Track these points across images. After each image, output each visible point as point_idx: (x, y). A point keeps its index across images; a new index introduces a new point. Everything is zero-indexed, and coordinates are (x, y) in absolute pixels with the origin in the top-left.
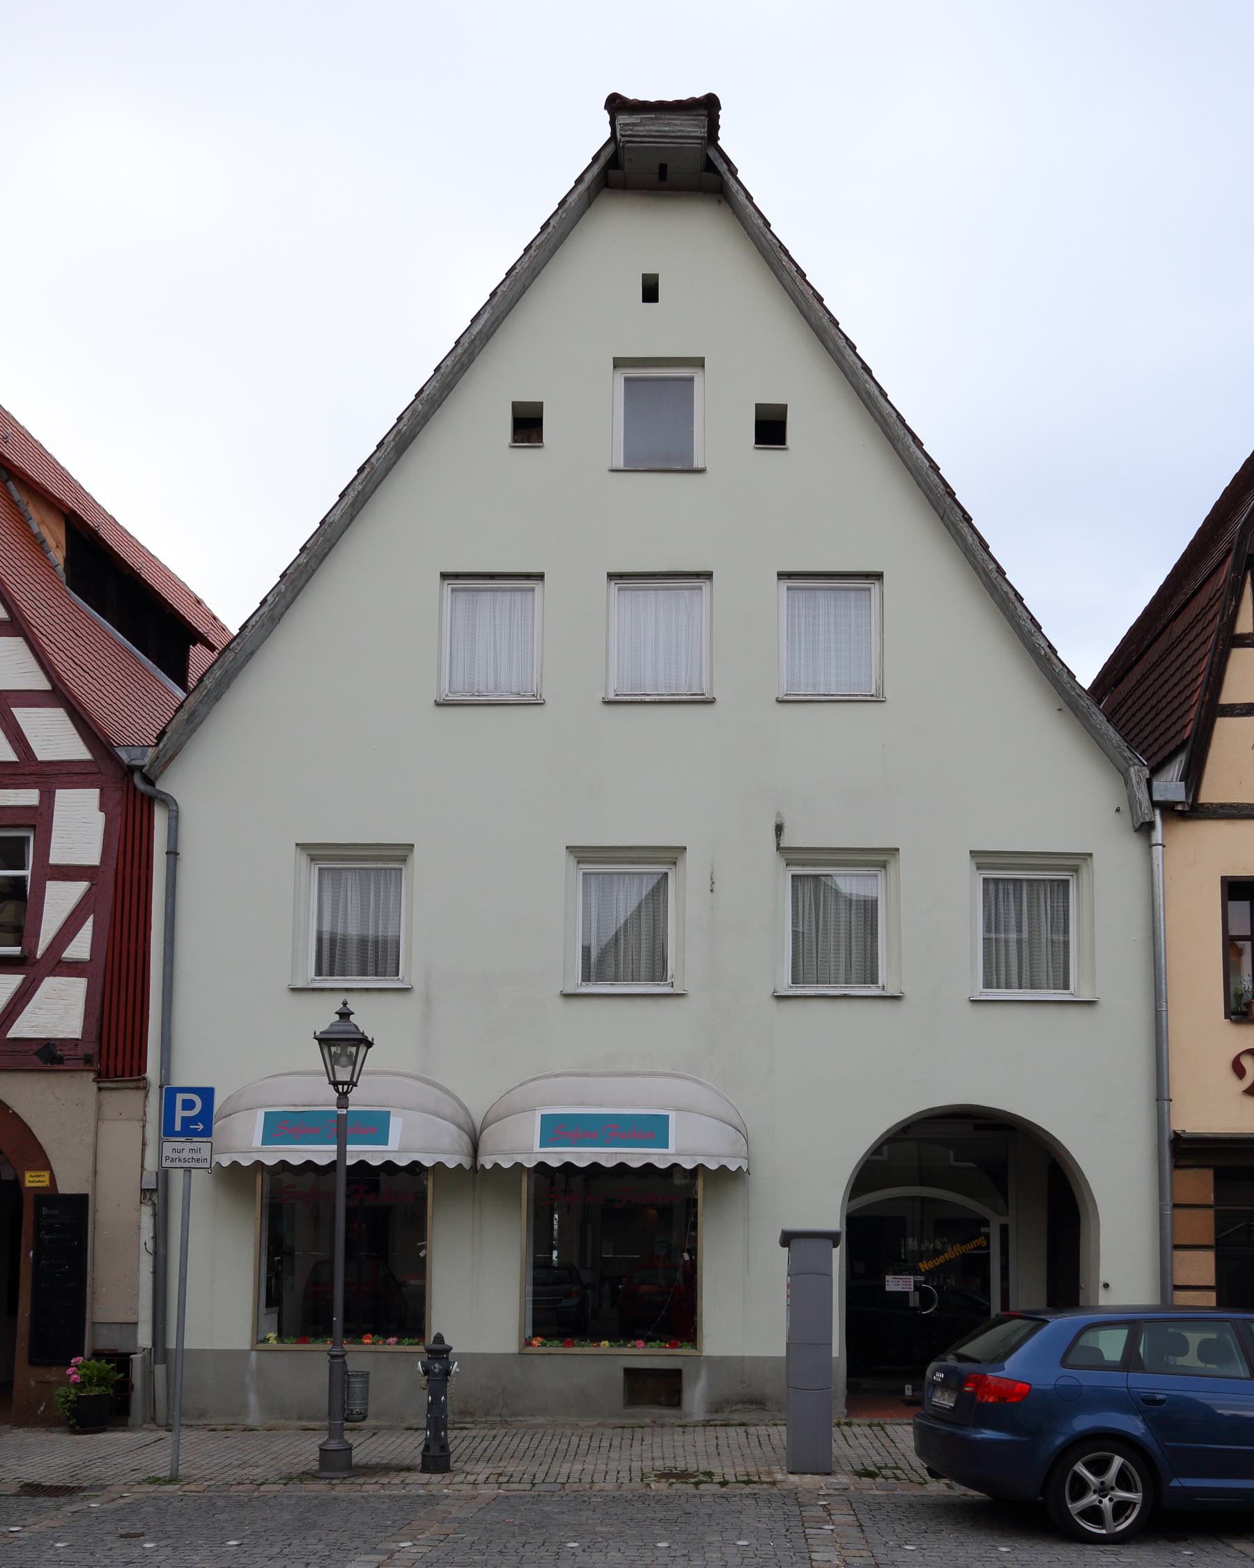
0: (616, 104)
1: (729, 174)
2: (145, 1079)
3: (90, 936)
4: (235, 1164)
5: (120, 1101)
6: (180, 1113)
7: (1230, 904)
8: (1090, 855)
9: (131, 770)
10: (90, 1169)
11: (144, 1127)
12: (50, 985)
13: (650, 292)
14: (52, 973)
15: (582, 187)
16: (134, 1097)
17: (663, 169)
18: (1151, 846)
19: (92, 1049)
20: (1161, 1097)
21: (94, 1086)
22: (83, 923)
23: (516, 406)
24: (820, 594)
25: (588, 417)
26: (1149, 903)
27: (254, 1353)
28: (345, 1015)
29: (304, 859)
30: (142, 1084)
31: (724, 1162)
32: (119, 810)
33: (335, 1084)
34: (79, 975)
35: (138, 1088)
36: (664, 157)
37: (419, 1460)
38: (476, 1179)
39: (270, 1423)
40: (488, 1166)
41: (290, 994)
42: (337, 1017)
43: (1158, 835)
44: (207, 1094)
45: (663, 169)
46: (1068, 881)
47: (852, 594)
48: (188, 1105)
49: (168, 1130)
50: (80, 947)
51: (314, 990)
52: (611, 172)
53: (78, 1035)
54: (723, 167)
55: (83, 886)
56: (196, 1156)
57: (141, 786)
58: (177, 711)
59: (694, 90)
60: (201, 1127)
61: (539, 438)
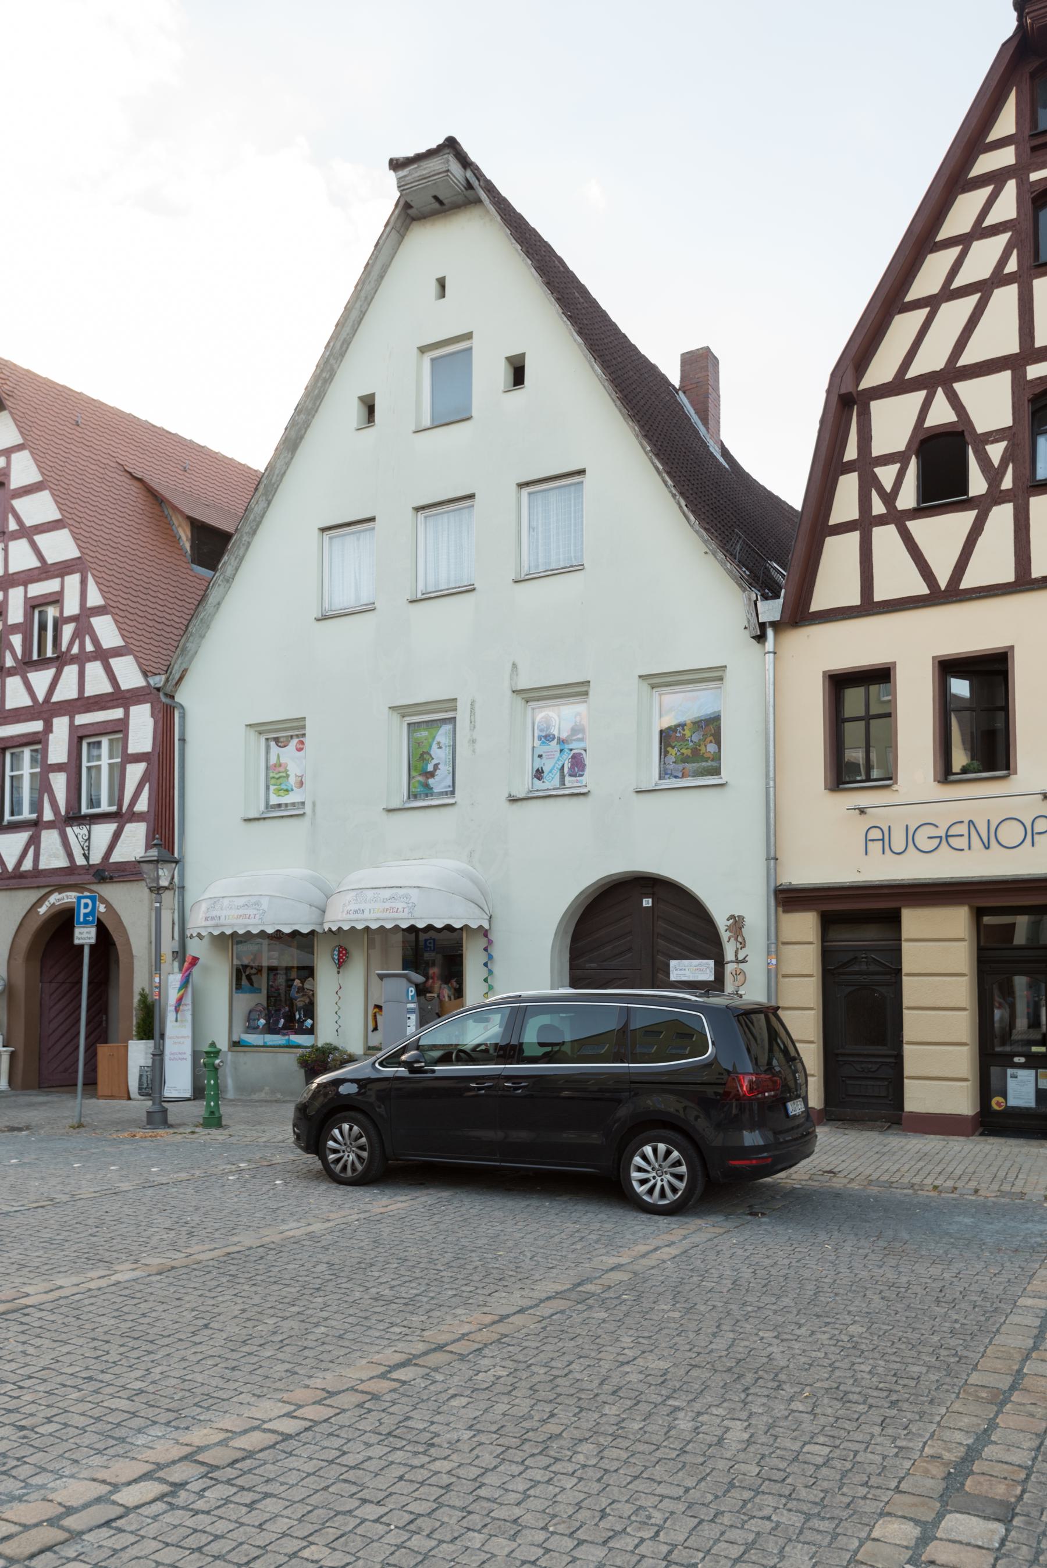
0: (396, 165)
4: (223, 933)
12: (129, 827)
14: (130, 821)
15: (388, 229)
20: (773, 859)
24: (551, 493)
29: (645, 686)
32: (161, 715)
36: (441, 187)
43: (770, 644)
50: (142, 805)
51: (264, 819)
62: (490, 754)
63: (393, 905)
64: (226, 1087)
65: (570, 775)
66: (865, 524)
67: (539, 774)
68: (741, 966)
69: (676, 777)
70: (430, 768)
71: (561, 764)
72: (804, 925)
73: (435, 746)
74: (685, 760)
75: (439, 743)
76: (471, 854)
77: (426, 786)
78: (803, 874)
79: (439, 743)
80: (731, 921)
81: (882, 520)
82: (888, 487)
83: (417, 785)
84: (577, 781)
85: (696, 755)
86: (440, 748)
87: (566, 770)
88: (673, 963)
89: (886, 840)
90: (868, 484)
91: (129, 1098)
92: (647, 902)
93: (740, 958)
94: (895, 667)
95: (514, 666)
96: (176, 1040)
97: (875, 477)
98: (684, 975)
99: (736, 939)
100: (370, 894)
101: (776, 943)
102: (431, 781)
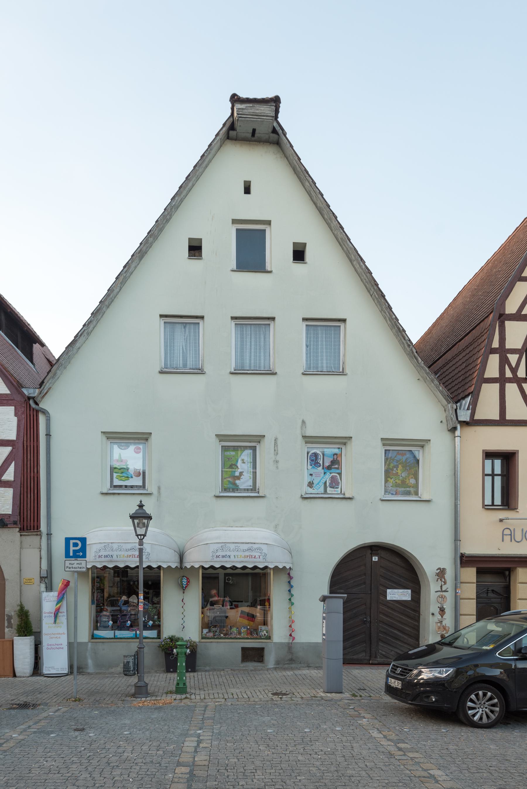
0: (235, 99)
1: (282, 134)
2: (40, 531)
3: (13, 470)
5: (30, 540)
6: (72, 548)
7: (486, 461)
8: (430, 440)
9: (29, 398)
10: (19, 569)
11: (40, 551)
13: (247, 190)
16: (36, 539)
17: (254, 131)
18: (455, 437)
19: (17, 518)
20: (457, 539)
21: (19, 534)
22: (10, 465)
23: (190, 240)
25: (222, 247)
26: (456, 462)
27: (90, 644)
28: (141, 506)
29: (104, 439)
30: (39, 533)
31: (277, 564)
33: (137, 535)
34: (9, 487)
35: (37, 535)
36: (254, 126)
37: (174, 689)
38: (182, 573)
39: (97, 671)
40: (188, 567)
41: (101, 495)
42: (138, 508)
43: (458, 433)
44: (83, 540)
45: (254, 131)
46: (256, 447)
47: (333, 328)
48: (75, 545)
49: (67, 555)
52: (231, 132)
53: (10, 512)
54: (280, 132)
55: (9, 449)
56: (80, 566)
57: (33, 405)
58: (48, 373)
59: (270, 95)
60: (81, 554)
61: (200, 255)
62: (284, 469)
63: (252, 554)
64: (87, 665)
65: (331, 487)
66: (502, 381)
67: (311, 485)
68: (444, 593)
69: (392, 494)
70: (237, 474)
71: (324, 480)
72: (470, 574)
73: (240, 461)
74: (397, 485)
75: (243, 460)
76: (276, 526)
77: (235, 484)
78: (472, 548)
79: (243, 460)
80: (439, 571)
81: (510, 380)
82: (514, 365)
83: (227, 483)
84: (335, 491)
85: (404, 483)
86: (244, 463)
87: (328, 484)
88: (389, 591)
89: (512, 536)
90: (504, 362)
91: (15, 675)
92: (375, 559)
93: (444, 589)
94: (518, 453)
95: (303, 422)
96: (53, 636)
97: (507, 359)
98: (395, 597)
99: (441, 580)
100: (232, 546)
101: (457, 582)
102: (237, 482)
